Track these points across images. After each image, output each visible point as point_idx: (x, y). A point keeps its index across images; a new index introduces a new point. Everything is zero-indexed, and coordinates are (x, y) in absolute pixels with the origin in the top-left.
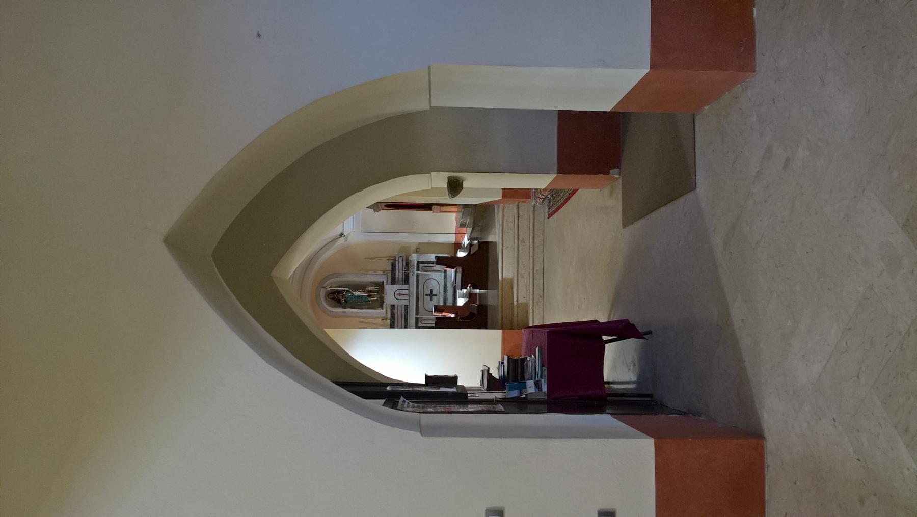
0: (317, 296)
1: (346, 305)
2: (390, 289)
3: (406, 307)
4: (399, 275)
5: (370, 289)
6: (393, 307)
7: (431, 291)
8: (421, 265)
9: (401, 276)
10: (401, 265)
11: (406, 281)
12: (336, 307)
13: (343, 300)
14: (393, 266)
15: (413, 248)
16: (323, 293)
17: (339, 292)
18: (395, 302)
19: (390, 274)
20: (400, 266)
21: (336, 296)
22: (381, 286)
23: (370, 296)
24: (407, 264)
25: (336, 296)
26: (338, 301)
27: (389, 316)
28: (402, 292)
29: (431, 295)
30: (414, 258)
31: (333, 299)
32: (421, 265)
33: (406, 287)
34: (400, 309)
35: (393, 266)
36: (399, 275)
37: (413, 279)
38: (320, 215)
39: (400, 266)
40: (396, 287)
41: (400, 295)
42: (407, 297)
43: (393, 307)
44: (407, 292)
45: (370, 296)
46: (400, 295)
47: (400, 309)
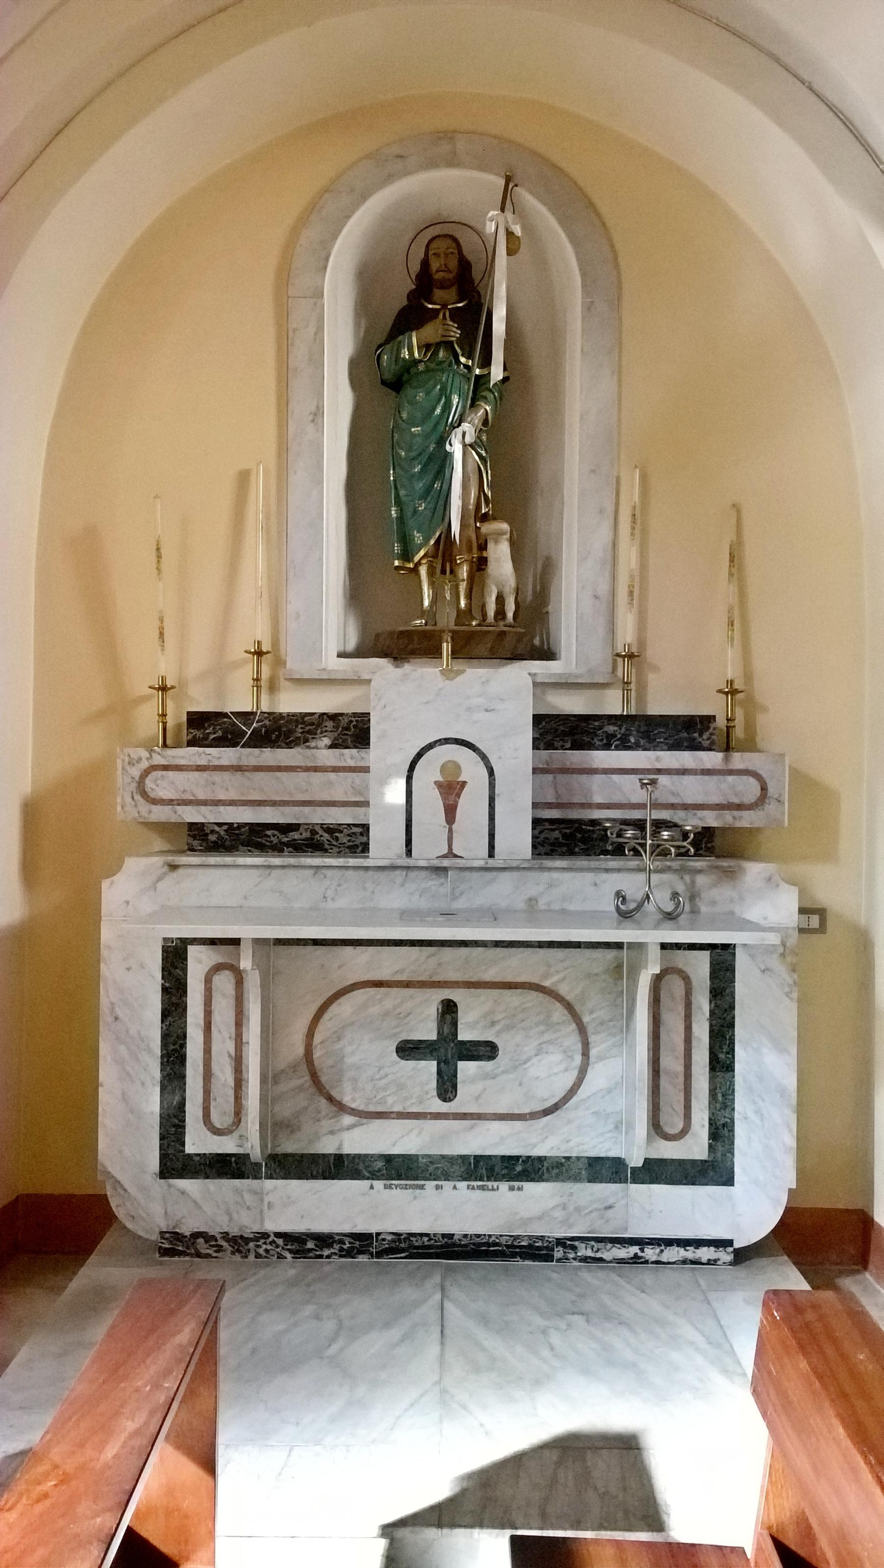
0: (443, 147)
1: (384, 379)
2: (498, 702)
3: (354, 841)
4: (614, 781)
5: (500, 556)
6: (354, 731)
7: (486, 1051)
8: (197, 1142)
9: (599, 790)
10: (692, 789)
11: (566, 837)
12: (368, 280)
13: (412, 347)
14: (688, 732)
15: (830, 891)
16: (462, 190)
17: (473, 316)
18: (388, 748)
19: (612, 704)
20: (689, 782)
21: (446, 298)
22: (523, 636)
23: (444, 553)
24: (713, 845)
25: (446, 298)
26: (411, 317)
27: (291, 702)
28: (472, 806)
29: (449, 1051)
30: (761, 908)
31: (425, 283)
32: (197, 1142)
33: (516, 837)
34: (340, 787)
35: (688, 732)
36: (614, 781)
37: (587, 891)
38: (348, 474)
39: (689, 782)
40: (516, 753)
41: (451, 790)
42: (429, 845)
43: (354, 731)
44: (471, 844)
45: (444, 553)
46: (451, 790)
47: (340, 787)
